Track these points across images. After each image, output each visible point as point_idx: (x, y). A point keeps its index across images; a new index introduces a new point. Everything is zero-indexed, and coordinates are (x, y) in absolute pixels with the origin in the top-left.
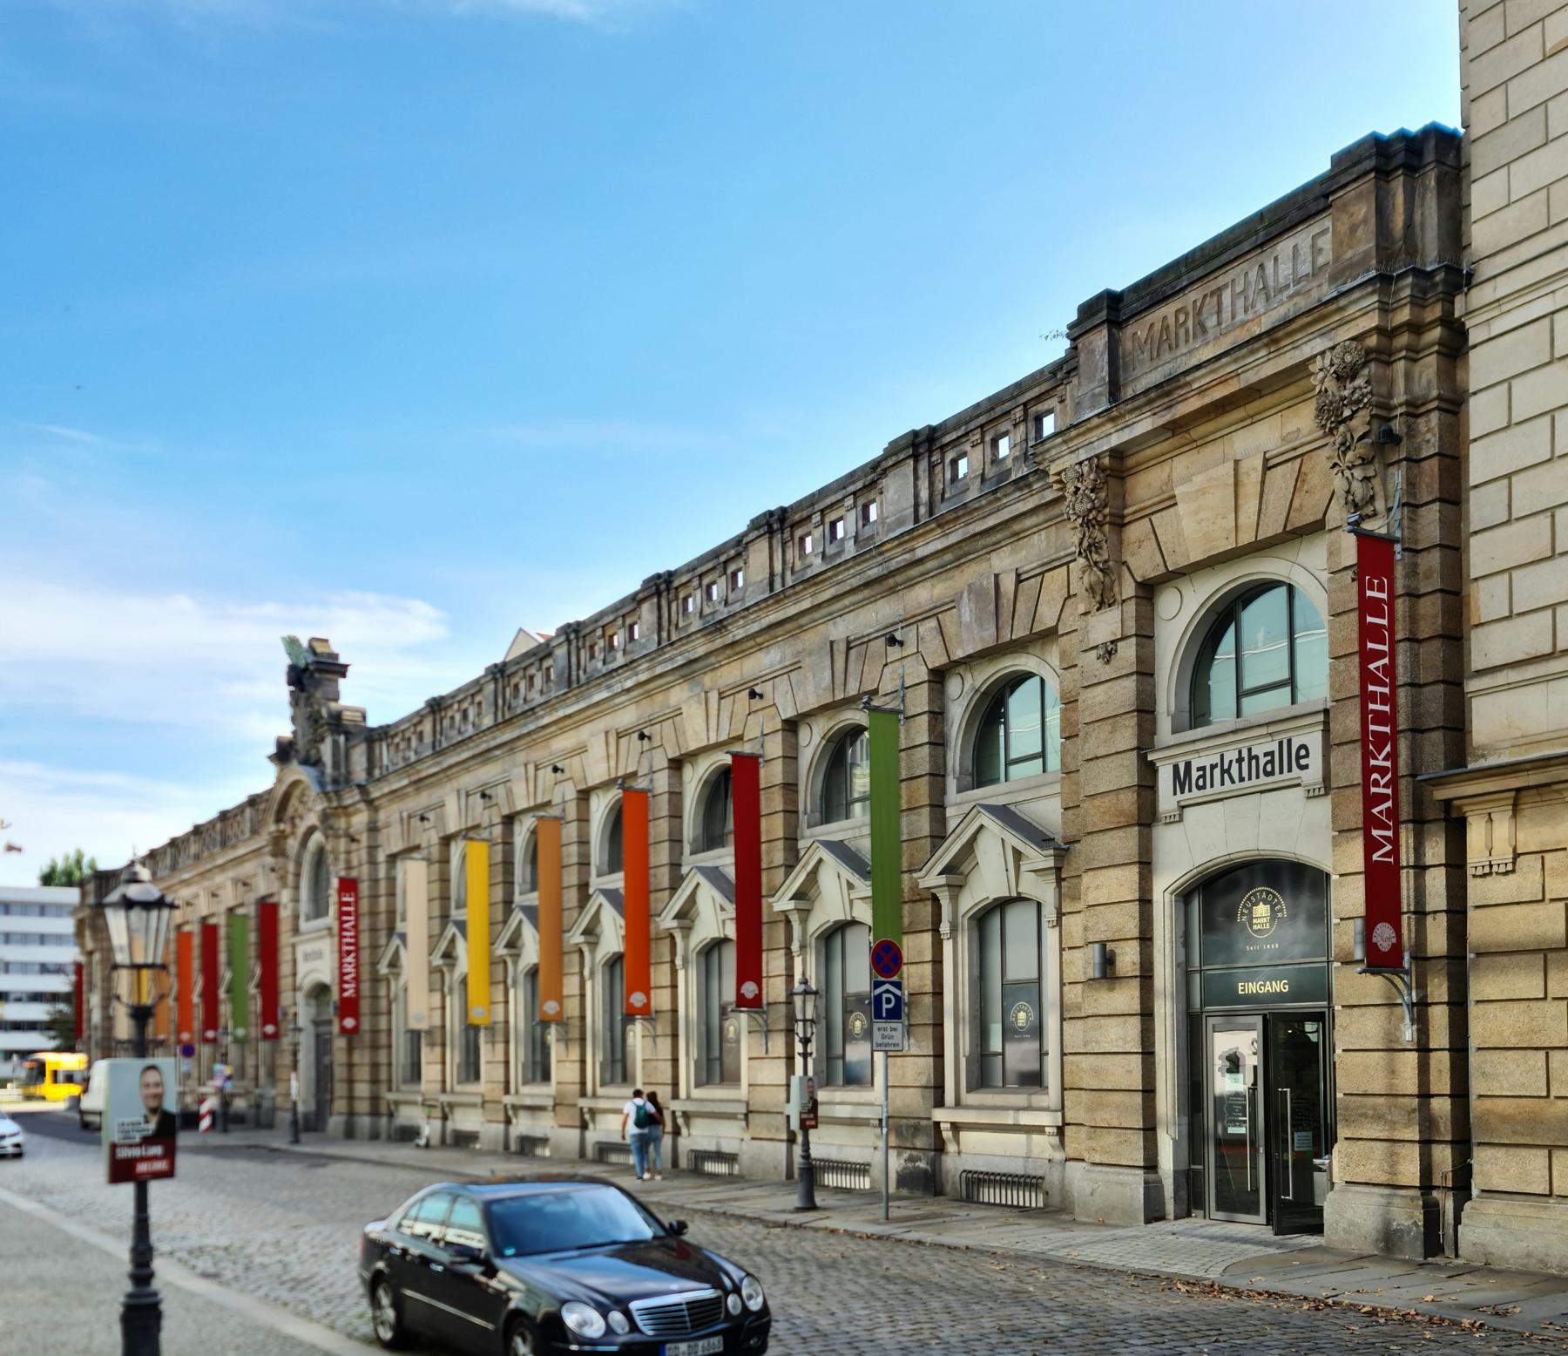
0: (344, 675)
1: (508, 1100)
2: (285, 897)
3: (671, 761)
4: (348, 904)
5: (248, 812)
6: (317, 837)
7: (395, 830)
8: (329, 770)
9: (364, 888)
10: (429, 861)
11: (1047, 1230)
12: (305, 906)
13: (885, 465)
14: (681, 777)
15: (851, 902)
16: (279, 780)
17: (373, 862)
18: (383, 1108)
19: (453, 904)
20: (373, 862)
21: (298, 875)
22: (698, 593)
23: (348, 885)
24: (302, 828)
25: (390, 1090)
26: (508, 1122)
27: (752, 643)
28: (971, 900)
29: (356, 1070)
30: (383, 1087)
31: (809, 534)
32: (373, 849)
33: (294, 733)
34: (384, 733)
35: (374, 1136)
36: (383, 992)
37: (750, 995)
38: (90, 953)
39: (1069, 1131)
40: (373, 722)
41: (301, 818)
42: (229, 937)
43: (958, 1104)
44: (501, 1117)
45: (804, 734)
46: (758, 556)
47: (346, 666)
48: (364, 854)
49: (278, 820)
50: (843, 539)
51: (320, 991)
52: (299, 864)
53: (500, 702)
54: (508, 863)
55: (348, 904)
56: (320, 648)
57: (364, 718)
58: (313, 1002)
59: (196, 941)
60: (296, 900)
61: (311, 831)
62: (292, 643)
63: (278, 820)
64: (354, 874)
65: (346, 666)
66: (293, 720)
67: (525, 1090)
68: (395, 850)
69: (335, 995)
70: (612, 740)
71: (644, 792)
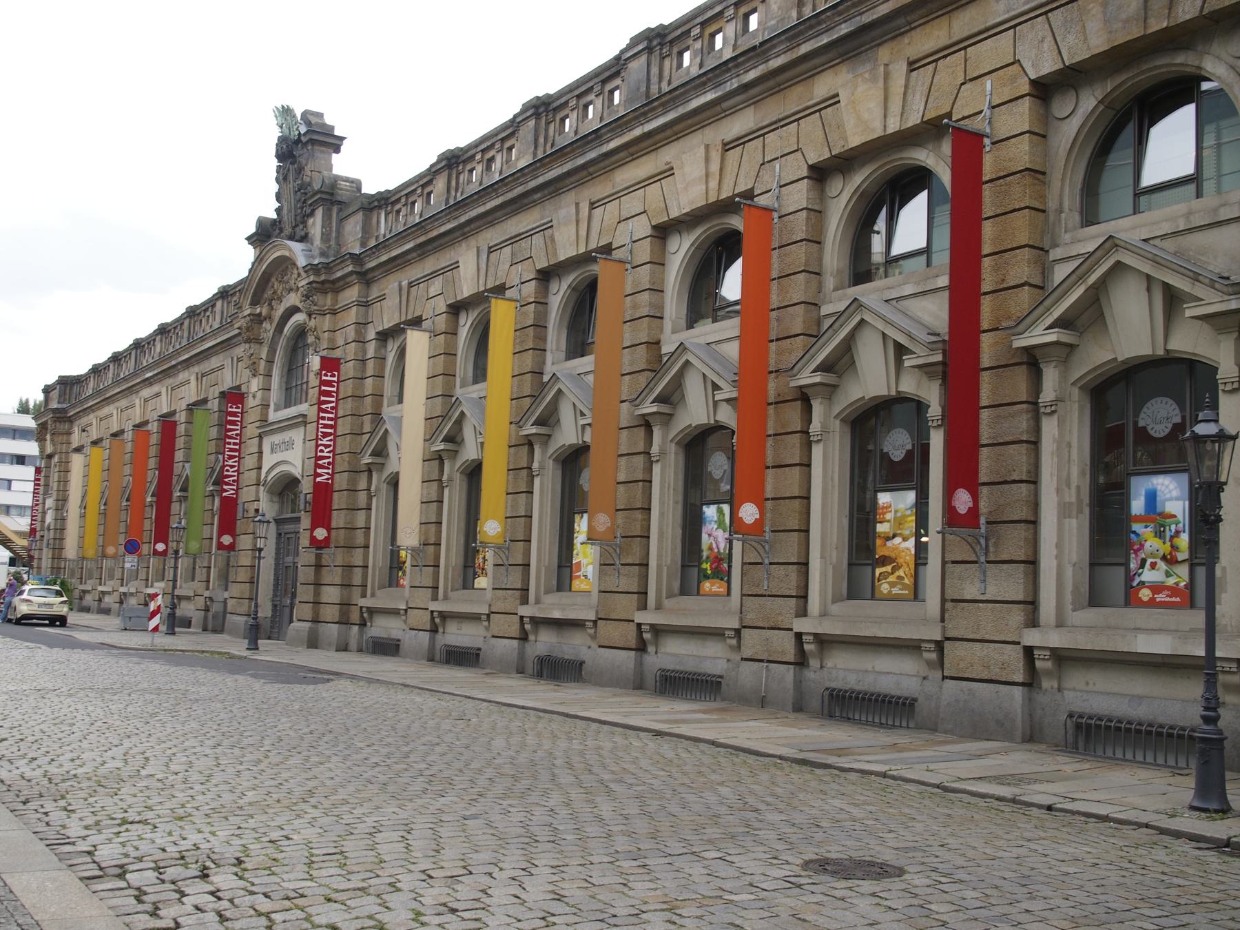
0: (333, 143)
1: (525, 611)
2: (255, 385)
3: (812, 168)
4: (329, 384)
5: (219, 304)
6: (299, 318)
7: (392, 302)
8: (317, 241)
9: (348, 369)
10: (434, 334)
11: (1061, 759)
12: (275, 395)
13: (518, 120)
14: (457, 322)
15: (716, 403)
16: (258, 260)
17: (361, 341)
18: (355, 616)
19: (458, 380)
20: (361, 341)
21: (270, 362)
22: (599, 102)
23: (330, 364)
24: (280, 310)
25: (364, 596)
26: (524, 638)
27: (584, 173)
28: (1098, 355)
29: (311, 578)
30: (357, 592)
31: (719, 31)
32: (362, 325)
33: (278, 211)
34: (384, 201)
35: (343, 648)
36: (363, 484)
37: (320, 538)
38: (50, 457)
39: (746, 633)
40: (369, 188)
41: (280, 300)
42: (188, 435)
43: (659, 607)
44: (514, 630)
45: (554, 286)
46: (440, 184)
47: (342, 139)
48: (351, 333)
49: (254, 303)
50: (689, 67)
51: (286, 487)
52: (272, 351)
53: (541, 140)
54: (540, 326)
55: (329, 384)
56: (314, 120)
57: (359, 189)
58: (276, 499)
59: (154, 439)
60: (267, 389)
61: (294, 310)
62: (286, 112)
63: (254, 303)
64: (337, 354)
65: (342, 139)
66: (278, 197)
67: (550, 599)
68: (387, 324)
69: (306, 487)
70: (715, 156)
71: (768, 210)
